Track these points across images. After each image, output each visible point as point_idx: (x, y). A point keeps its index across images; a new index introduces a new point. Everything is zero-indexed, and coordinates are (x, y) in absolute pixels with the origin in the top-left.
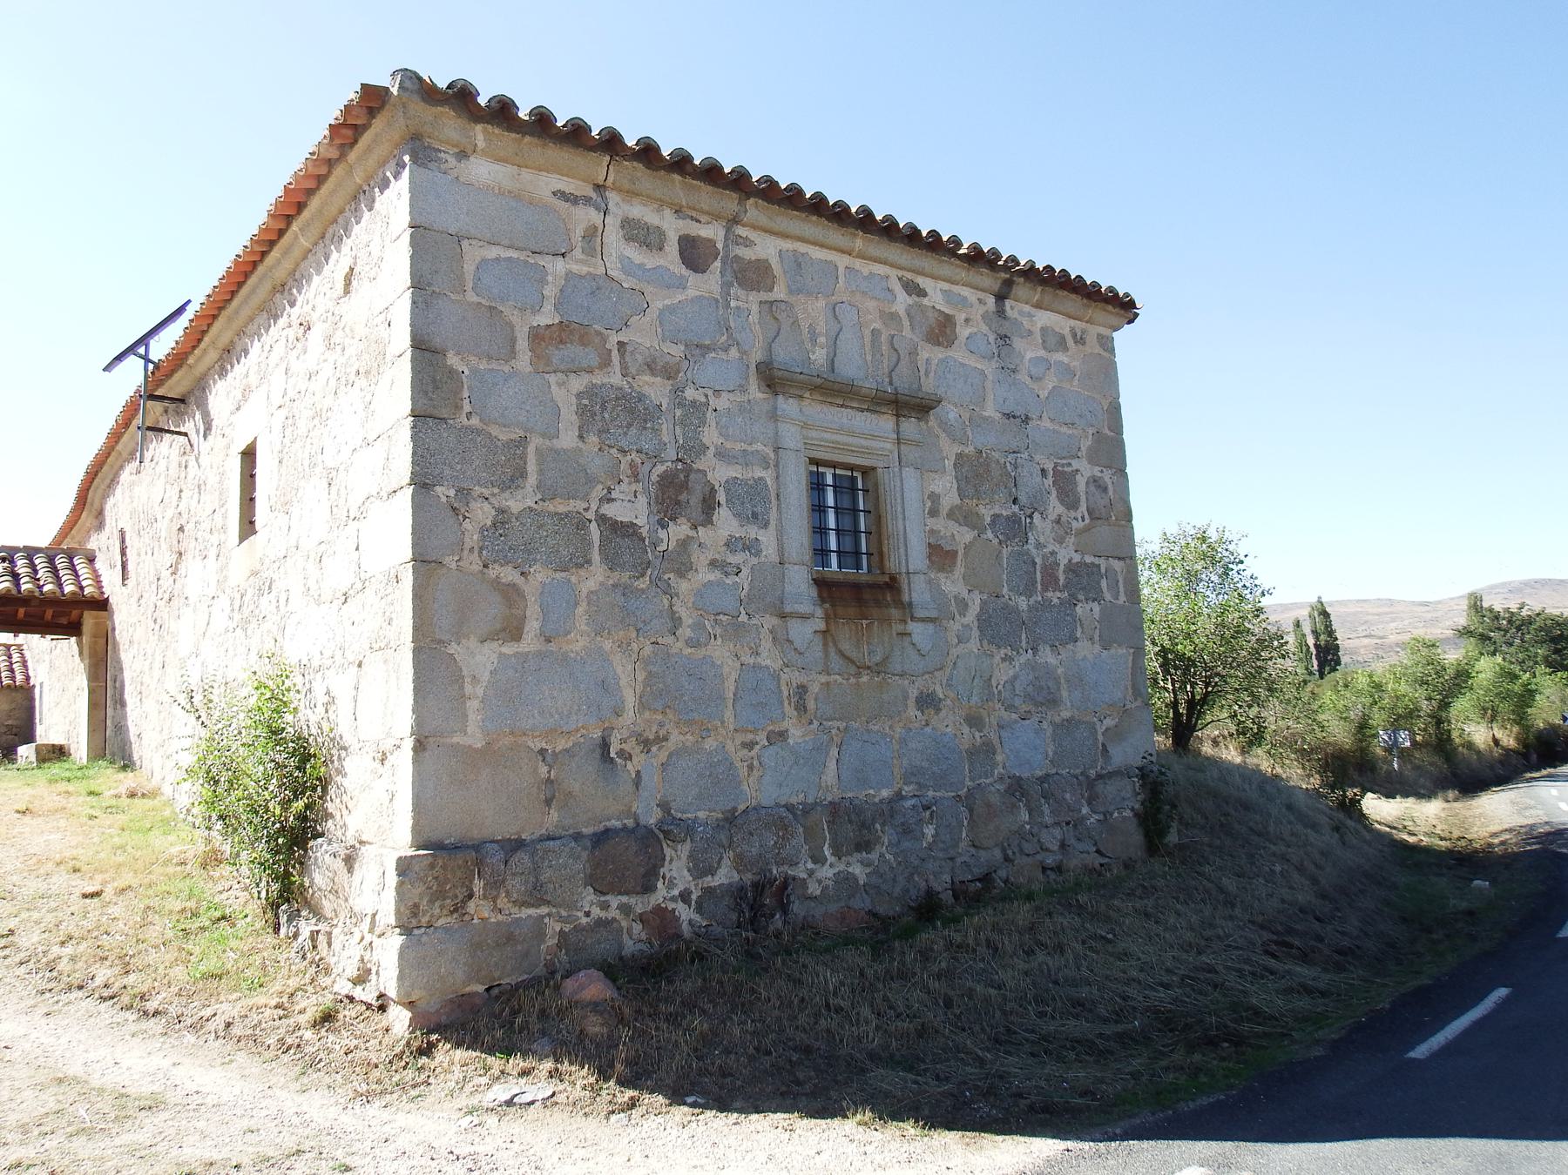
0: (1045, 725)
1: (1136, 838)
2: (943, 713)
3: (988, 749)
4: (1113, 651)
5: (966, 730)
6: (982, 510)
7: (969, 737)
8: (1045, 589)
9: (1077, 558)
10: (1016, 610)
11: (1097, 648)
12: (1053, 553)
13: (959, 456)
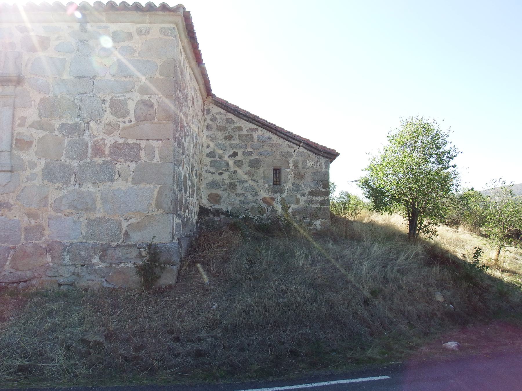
0: (81, 219)
1: (134, 280)
2: (12, 211)
3: (40, 228)
4: (142, 186)
5: (26, 219)
6: (53, 122)
7: (26, 222)
8: (94, 155)
9: (121, 141)
10: (244, 217)
11: (130, 184)
12: (103, 139)
13: (42, 100)
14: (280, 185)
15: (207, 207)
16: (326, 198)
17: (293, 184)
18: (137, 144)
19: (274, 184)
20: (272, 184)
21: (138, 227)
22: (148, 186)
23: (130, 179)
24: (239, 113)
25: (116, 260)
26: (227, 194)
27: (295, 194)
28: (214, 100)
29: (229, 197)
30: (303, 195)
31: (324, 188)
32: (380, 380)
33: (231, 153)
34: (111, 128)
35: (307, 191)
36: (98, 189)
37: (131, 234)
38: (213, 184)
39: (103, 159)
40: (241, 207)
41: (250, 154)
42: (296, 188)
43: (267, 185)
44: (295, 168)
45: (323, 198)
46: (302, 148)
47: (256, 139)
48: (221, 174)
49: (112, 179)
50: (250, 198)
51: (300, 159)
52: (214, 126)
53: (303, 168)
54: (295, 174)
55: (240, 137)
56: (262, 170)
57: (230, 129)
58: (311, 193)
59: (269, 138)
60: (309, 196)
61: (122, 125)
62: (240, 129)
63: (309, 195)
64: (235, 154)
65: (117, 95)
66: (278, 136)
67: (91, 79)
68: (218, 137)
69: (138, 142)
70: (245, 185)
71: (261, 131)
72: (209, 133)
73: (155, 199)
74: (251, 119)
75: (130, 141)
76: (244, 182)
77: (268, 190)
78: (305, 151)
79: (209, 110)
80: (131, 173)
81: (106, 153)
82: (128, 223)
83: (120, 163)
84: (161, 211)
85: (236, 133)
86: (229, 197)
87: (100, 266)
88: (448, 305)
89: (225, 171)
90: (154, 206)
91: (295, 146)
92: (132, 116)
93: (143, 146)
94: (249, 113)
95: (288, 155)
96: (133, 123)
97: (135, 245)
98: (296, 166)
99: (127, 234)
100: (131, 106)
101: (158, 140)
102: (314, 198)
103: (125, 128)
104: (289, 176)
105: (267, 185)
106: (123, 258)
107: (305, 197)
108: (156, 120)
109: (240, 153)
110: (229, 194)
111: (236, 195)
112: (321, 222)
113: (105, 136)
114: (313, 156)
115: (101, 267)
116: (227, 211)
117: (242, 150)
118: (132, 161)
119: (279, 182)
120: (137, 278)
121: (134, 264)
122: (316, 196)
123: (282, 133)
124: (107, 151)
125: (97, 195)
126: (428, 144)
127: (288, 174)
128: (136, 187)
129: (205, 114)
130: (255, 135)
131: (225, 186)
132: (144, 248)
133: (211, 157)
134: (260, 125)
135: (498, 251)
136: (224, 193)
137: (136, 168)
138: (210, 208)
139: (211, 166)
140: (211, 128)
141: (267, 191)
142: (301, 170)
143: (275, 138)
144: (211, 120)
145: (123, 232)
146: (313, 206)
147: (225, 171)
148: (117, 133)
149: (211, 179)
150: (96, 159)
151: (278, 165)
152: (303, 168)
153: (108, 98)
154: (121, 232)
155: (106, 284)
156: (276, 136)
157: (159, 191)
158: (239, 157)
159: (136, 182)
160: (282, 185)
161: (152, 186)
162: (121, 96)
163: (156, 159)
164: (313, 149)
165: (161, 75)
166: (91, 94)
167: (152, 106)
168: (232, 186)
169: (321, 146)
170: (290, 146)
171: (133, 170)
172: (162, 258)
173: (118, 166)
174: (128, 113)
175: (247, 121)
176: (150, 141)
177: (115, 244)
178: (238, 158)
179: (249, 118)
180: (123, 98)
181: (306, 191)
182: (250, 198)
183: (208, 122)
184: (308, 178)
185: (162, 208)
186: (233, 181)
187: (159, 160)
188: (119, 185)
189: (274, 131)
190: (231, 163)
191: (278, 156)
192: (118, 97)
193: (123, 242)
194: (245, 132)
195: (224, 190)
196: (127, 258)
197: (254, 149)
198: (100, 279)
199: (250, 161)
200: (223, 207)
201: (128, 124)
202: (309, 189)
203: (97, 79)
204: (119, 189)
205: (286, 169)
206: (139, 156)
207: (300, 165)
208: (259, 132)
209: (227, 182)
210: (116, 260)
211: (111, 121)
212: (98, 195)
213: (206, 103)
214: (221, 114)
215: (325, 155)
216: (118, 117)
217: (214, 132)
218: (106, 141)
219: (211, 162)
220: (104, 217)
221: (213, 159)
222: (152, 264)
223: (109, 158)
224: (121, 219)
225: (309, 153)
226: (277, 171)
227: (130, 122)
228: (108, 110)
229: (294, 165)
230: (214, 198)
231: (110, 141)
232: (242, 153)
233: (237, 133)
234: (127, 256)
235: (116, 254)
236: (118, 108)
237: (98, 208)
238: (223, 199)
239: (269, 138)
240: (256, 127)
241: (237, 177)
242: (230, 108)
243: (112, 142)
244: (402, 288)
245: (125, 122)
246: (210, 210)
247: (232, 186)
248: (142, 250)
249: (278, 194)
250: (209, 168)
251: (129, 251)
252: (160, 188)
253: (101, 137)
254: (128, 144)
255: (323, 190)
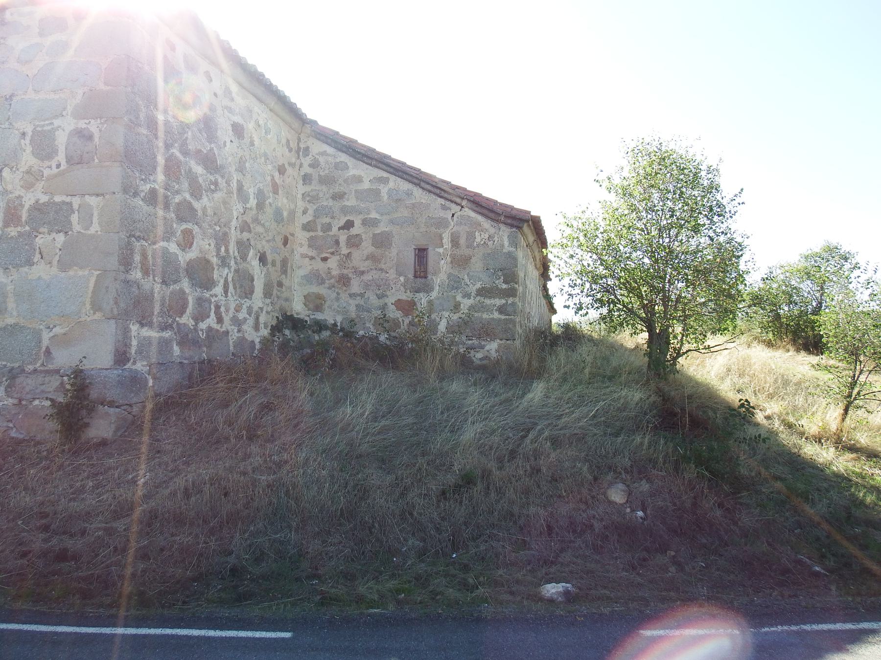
1: (49, 430)
4: (71, 273)
9: (44, 199)
11: (54, 270)
14: (426, 277)
15: (301, 316)
16: (509, 302)
17: (449, 276)
18: (67, 203)
19: (415, 277)
20: (411, 276)
21: (64, 340)
22: (80, 273)
23: (55, 262)
24: (354, 150)
25: (27, 393)
26: (335, 294)
27: (453, 293)
28: (314, 131)
29: (337, 299)
30: (467, 295)
31: (505, 282)
32: (265, 639)
33: (342, 223)
34: (31, 178)
35: (474, 288)
36: (10, 278)
37: (55, 353)
38: (316, 277)
39: (19, 229)
40: (358, 316)
41: (374, 223)
42: (455, 283)
43: (402, 279)
44: (452, 246)
45: (504, 301)
46: (466, 209)
47: (386, 197)
48: (325, 259)
49: (30, 263)
50: (374, 301)
51: (463, 230)
52: (315, 177)
53: (468, 247)
54: (453, 257)
55: (359, 194)
56: (394, 251)
57: (341, 181)
58: (481, 292)
59: (408, 194)
60: (478, 298)
61: (47, 172)
62: (359, 179)
63: (477, 295)
64: (349, 225)
65: (42, 123)
66: (423, 188)
67: (6, 99)
68: (321, 195)
69: (68, 199)
70: (367, 277)
71: (395, 182)
72: (308, 188)
73: (90, 295)
74: (376, 160)
75: (58, 199)
76: (363, 273)
77: (404, 286)
78: (472, 214)
79: (307, 149)
80: (58, 251)
81: (24, 219)
82: (51, 334)
83: (41, 236)
84: (98, 316)
85: (351, 186)
86: (337, 299)
87: (5, 402)
88: (633, 511)
89: (332, 253)
90: (88, 306)
91: (453, 206)
92: (61, 157)
93: (75, 206)
94: (374, 150)
95: (442, 223)
96: (62, 168)
97: (57, 371)
98: (455, 242)
99: (48, 352)
100: (61, 139)
101: (98, 195)
102: (488, 302)
103: (50, 178)
104: (443, 262)
105: (402, 279)
106: (38, 391)
107: (470, 298)
108: (96, 161)
109: (358, 222)
110: (338, 294)
111: (351, 295)
112: (500, 346)
113: (22, 192)
114: (486, 224)
115: (7, 405)
116: (335, 325)
117: (362, 217)
118: (59, 232)
119: (426, 272)
120: (53, 425)
121: (52, 400)
122: (490, 298)
123: (428, 184)
124: (24, 216)
125: (9, 288)
126: (678, 191)
127: (441, 257)
128: (63, 274)
129: (301, 157)
130: (384, 190)
131: (332, 281)
132: (67, 375)
133: (309, 231)
134: (392, 170)
135: (843, 407)
136: (329, 292)
137: (65, 242)
138: (307, 319)
139: (310, 246)
140: (311, 180)
141: (402, 288)
142: (464, 251)
143: (417, 192)
144: (310, 166)
145: (44, 349)
146: (485, 316)
147: (332, 253)
148: (40, 185)
149: (310, 268)
150: (9, 229)
151: (422, 243)
152: (468, 247)
153: (29, 130)
154: (40, 348)
155: (16, 432)
156: (420, 190)
157: (96, 281)
158: (356, 230)
159: (64, 266)
160: (430, 277)
161: (86, 273)
162: (47, 125)
163: (95, 228)
164: (486, 212)
165: (106, 84)
166: (7, 125)
167: (90, 138)
168: (344, 281)
169: (501, 204)
170: (444, 208)
171: (59, 246)
172: (94, 394)
173: (39, 241)
174: (56, 152)
175: (370, 165)
176: (87, 196)
177: (30, 368)
178: (354, 231)
179: (372, 159)
180: (49, 128)
181: (473, 289)
182: (374, 301)
183: (306, 169)
184: (477, 265)
185: (100, 309)
186: (345, 272)
187: (99, 229)
188: (40, 271)
189: (416, 181)
190: (343, 239)
191: (423, 226)
192: (43, 126)
193: (43, 365)
194: (366, 185)
195: (329, 288)
196: (43, 391)
197: (382, 215)
198: (5, 424)
199: (374, 235)
200: (328, 316)
201: (55, 171)
202: (478, 285)
203: (15, 99)
204: (40, 278)
205: (437, 250)
206: (70, 223)
207: (462, 241)
208: (391, 184)
209: (335, 272)
210: (27, 393)
211: (31, 167)
212: (10, 288)
213: (302, 136)
214: (328, 155)
215: (509, 221)
216: (42, 160)
217: (315, 186)
218: (24, 200)
219: (311, 239)
220: (16, 324)
221: (312, 234)
222: (77, 403)
223: (27, 228)
224: (41, 327)
225: (480, 218)
226: (421, 253)
227: (58, 166)
228: (29, 149)
229: (452, 241)
230: (316, 302)
231: (29, 200)
232: (360, 222)
233: (354, 187)
234: (43, 387)
235: (28, 384)
236: (43, 146)
237: (9, 309)
238: (328, 303)
239: (409, 194)
240: (385, 175)
241: (351, 265)
242: (340, 144)
243: (33, 201)
244: (539, 471)
245: (50, 167)
246: (306, 321)
247: (344, 281)
248: (65, 378)
249: (421, 295)
250: (305, 250)
251: (47, 379)
252: (98, 275)
253: (17, 193)
254: (55, 203)
255: (504, 286)
